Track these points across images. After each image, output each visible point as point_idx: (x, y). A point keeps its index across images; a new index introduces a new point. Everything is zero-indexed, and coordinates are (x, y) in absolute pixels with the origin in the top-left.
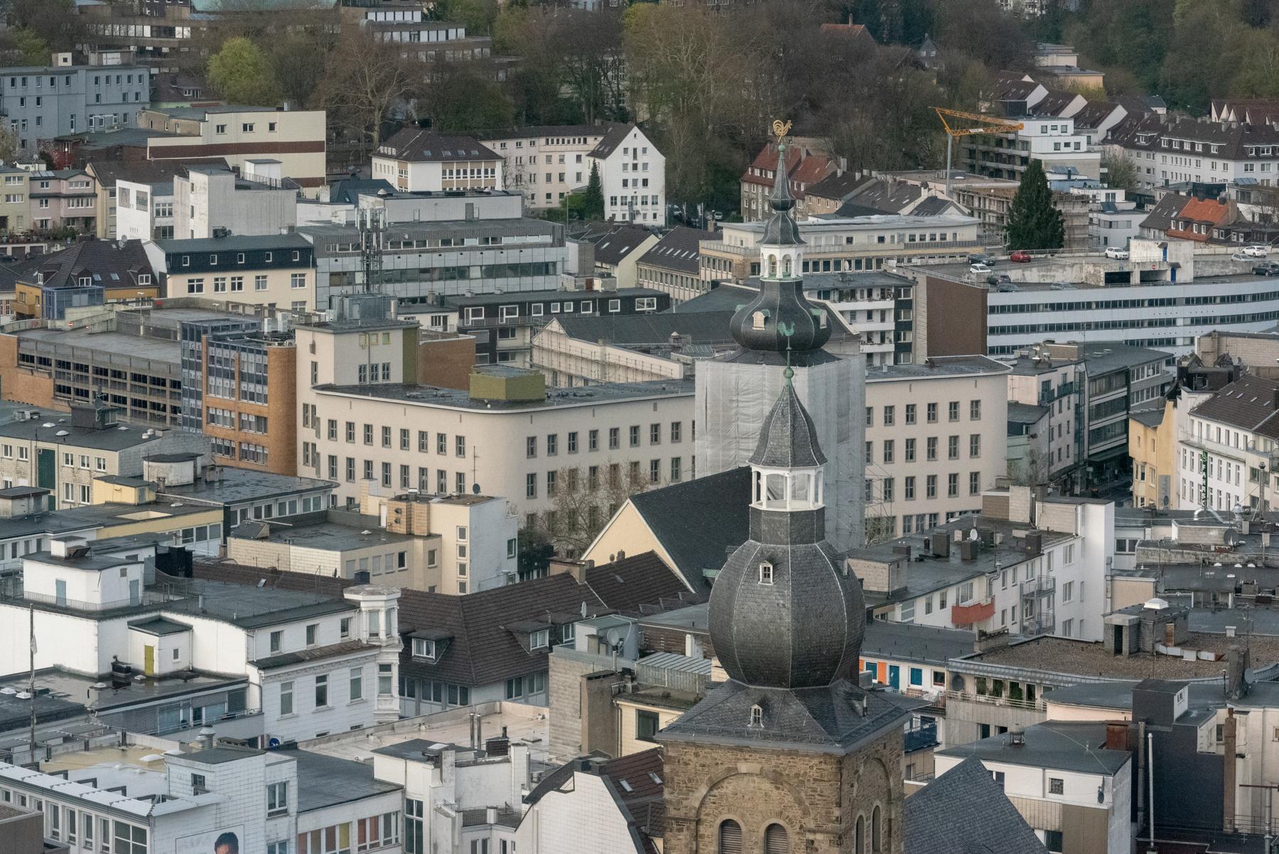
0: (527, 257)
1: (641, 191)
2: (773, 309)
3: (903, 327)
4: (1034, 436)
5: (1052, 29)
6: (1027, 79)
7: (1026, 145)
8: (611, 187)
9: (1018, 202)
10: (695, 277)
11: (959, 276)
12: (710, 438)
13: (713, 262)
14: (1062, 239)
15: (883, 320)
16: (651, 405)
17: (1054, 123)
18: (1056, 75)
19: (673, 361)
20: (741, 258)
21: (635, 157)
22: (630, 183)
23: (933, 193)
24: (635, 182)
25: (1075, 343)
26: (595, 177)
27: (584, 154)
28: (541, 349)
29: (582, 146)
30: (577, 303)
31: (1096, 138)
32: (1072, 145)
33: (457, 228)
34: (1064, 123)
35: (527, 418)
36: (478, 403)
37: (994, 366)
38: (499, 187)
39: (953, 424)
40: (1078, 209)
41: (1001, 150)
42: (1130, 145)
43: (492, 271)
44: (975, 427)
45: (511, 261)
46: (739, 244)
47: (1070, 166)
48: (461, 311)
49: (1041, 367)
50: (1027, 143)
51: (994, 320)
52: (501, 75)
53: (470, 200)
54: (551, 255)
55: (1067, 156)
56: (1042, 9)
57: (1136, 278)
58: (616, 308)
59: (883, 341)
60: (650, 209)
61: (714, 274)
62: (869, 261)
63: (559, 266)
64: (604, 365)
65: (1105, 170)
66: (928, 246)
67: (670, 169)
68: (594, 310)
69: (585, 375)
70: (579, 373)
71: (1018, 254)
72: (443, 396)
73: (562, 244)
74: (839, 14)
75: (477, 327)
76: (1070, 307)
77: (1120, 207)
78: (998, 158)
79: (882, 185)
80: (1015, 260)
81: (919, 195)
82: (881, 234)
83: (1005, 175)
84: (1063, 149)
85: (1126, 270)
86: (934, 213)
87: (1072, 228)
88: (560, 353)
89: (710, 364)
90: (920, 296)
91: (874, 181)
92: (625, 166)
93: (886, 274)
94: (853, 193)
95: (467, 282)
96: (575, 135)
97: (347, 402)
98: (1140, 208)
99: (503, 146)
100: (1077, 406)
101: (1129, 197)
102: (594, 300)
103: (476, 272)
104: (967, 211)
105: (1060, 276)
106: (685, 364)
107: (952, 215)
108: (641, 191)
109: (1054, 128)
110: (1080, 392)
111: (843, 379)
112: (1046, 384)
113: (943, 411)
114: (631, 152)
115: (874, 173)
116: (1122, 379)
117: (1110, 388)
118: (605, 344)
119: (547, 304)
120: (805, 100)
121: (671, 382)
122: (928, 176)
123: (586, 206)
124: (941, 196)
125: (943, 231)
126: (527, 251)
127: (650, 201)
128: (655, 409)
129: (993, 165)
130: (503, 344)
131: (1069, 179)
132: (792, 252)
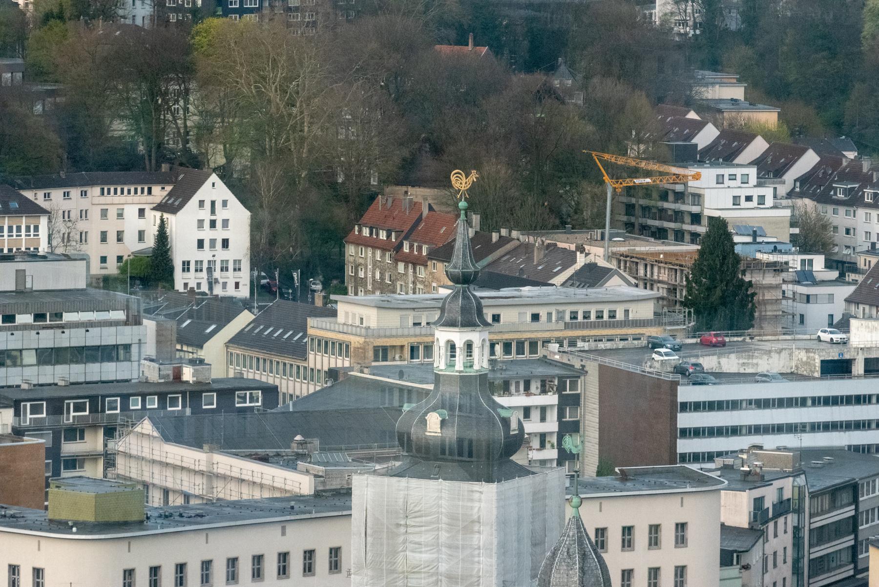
0: (94, 338)
1: (221, 254)
2: (451, 409)
3: (569, 428)
4: (746, 567)
5: (710, 48)
6: (692, 115)
7: (697, 198)
8: (182, 250)
9: (698, 268)
10: (302, 364)
11: (639, 363)
12: (370, 573)
13: (326, 345)
14: (752, 316)
15: (543, 419)
16: (278, 529)
17: (732, 171)
18: (720, 111)
19: (301, 472)
20: (362, 340)
21: (213, 212)
22: (207, 244)
23: (591, 259)
24: (213, 242)
25: (786, 449)
26: (162, 237)
27: (148, 208)
28: (128, 456)
29: (145, 198)
30: (162, 396)
31: (783, 190)
32: (755, 199)
33: (7, 301)
34: (745, 171)
35: (124, 545)
36: (60, 526)
37: (701, 480)
38: (43, 248)
39: (627, 554)
40: (769, 279)
41: (666, 205)
42: (824, 199)
43: (49, 356)
44: (681, 556)
45: (74, 344)
46: (358, 323)
47: (755, 225)
48: (16, 405)
49: (750, 480)
50: (699, 196)
51: (685, 420)
52: (39, 108)
53: (22, 266)
54: (126, 335)
55: (748, 214)
56: (695, 28)
57: (859, 368)
58: (210, 403)
59: (543, 446)
60: (231, 277)
61: (333, 361)
62: (520, 344)
63: (134, 350)
64: (211, 476)
65: (796, 231)
66: (593, 326)
67: (255, 226)
68: (184, 406)
69: (185, 489)
70: (178, 487)
71: (711, 336)
72: (13, 516)
73: (138, 322)
74: (452, 34)
75: (37, 429)
76: (782, 403)
77: (819, 277)
78: (662, 214)
79: (527, 248)
80: (706, 344)
81: (574, 261)
82: (535, 310)
83: (671, 236)
84: (744, 204)
85: (847, 357)
86: (592, 285)
87: (765, 302)
88: (154, 462)
89: (372, 479)
90: (590, 388)
91: (516, 243)
92: (201, 223)
93: (545, 361)
94: (490, 259)
95: (18, 369)
96: (139, 183)
97: (34, 543)
98: (841, 280)
99: (47, 196)
100: (797, 530)
101: (830, 264)
102: (184, 393)
103: (30, 358)
104: (633, 281)
105: (764, 365)
106: (316, 476)
107: (616, 286)
108: (221, 254)
109: (733, 177)
110: (799, 511)
111: (539, 496)
112: (758, 502)
113: (641, 537)
114: (208, 205)
115: (515, 234)
116: (846, 497)
117: (833, 507)
118: (211, 450)
119: (125, 398)
120: (427, 140)
121: (299, 498)
122: (581, 237)
123: (153, 269)
124: (602, 263)
125: (612, 307)
126: (94, 331)
127: (231, 266)
128: (284, 533)
129: (657, 223)
130: (69, 448)
131: (755, 242)
132: (476, 337)
